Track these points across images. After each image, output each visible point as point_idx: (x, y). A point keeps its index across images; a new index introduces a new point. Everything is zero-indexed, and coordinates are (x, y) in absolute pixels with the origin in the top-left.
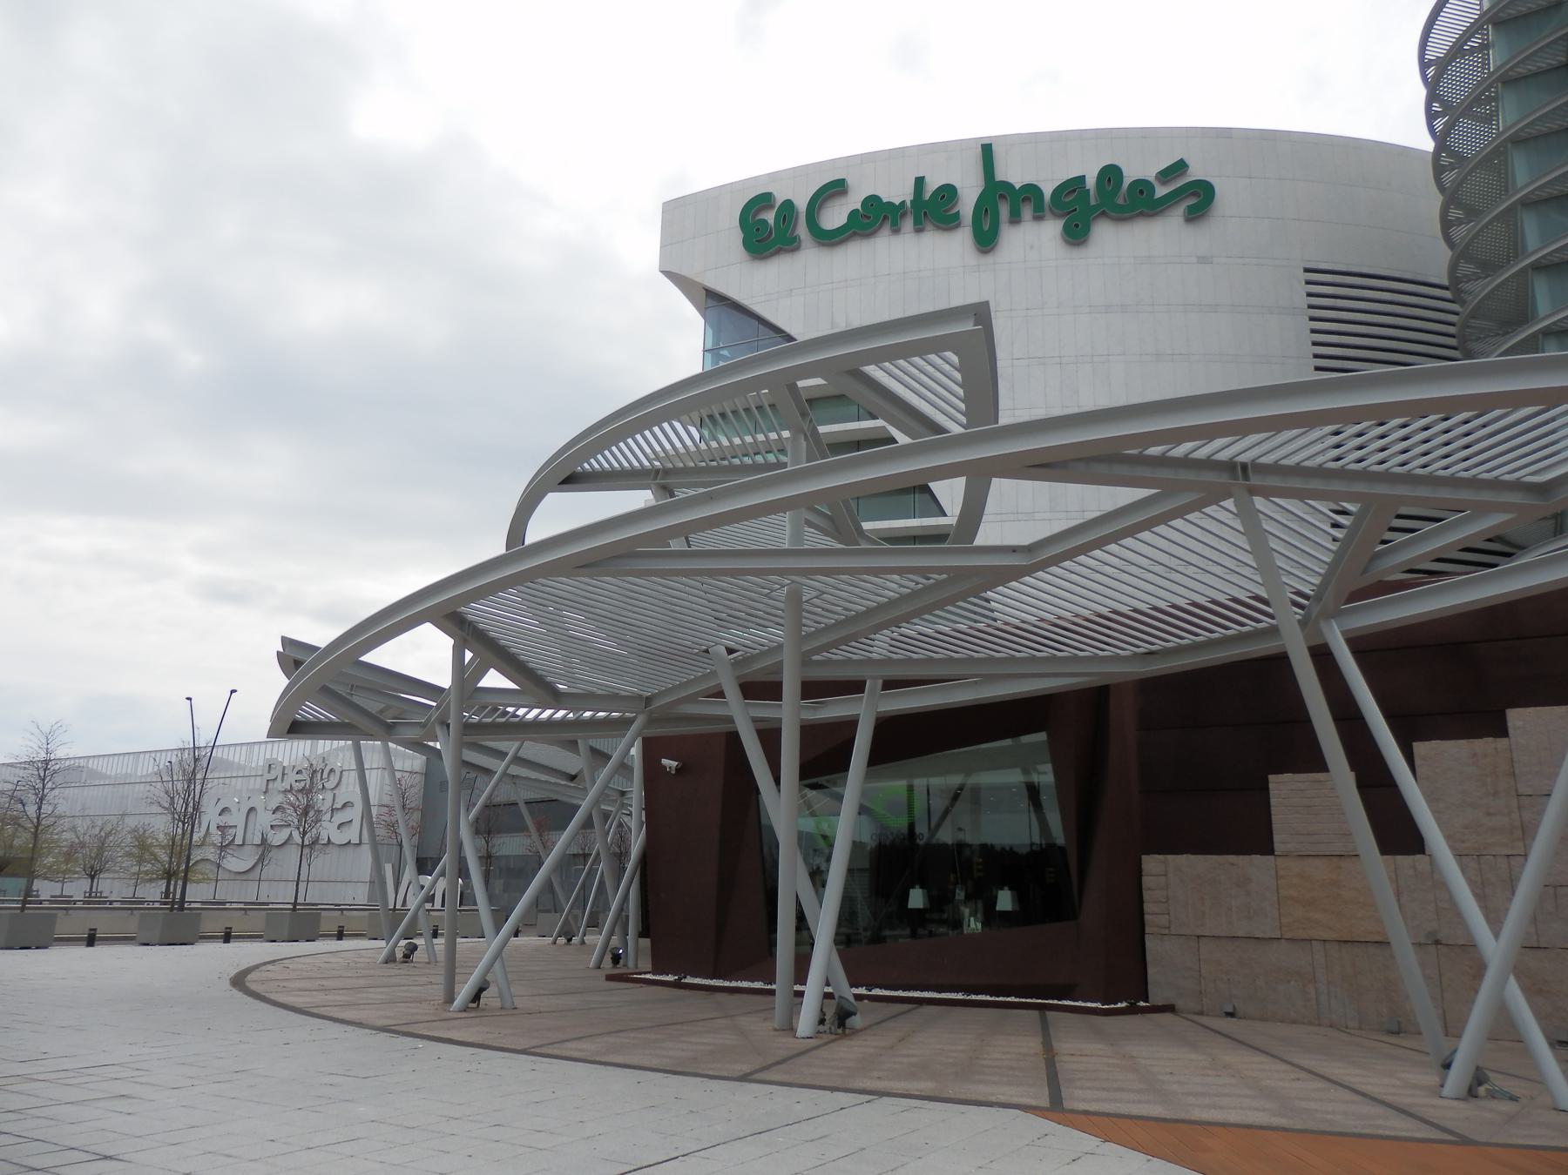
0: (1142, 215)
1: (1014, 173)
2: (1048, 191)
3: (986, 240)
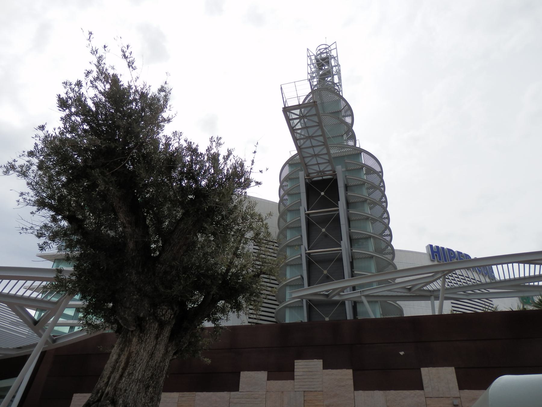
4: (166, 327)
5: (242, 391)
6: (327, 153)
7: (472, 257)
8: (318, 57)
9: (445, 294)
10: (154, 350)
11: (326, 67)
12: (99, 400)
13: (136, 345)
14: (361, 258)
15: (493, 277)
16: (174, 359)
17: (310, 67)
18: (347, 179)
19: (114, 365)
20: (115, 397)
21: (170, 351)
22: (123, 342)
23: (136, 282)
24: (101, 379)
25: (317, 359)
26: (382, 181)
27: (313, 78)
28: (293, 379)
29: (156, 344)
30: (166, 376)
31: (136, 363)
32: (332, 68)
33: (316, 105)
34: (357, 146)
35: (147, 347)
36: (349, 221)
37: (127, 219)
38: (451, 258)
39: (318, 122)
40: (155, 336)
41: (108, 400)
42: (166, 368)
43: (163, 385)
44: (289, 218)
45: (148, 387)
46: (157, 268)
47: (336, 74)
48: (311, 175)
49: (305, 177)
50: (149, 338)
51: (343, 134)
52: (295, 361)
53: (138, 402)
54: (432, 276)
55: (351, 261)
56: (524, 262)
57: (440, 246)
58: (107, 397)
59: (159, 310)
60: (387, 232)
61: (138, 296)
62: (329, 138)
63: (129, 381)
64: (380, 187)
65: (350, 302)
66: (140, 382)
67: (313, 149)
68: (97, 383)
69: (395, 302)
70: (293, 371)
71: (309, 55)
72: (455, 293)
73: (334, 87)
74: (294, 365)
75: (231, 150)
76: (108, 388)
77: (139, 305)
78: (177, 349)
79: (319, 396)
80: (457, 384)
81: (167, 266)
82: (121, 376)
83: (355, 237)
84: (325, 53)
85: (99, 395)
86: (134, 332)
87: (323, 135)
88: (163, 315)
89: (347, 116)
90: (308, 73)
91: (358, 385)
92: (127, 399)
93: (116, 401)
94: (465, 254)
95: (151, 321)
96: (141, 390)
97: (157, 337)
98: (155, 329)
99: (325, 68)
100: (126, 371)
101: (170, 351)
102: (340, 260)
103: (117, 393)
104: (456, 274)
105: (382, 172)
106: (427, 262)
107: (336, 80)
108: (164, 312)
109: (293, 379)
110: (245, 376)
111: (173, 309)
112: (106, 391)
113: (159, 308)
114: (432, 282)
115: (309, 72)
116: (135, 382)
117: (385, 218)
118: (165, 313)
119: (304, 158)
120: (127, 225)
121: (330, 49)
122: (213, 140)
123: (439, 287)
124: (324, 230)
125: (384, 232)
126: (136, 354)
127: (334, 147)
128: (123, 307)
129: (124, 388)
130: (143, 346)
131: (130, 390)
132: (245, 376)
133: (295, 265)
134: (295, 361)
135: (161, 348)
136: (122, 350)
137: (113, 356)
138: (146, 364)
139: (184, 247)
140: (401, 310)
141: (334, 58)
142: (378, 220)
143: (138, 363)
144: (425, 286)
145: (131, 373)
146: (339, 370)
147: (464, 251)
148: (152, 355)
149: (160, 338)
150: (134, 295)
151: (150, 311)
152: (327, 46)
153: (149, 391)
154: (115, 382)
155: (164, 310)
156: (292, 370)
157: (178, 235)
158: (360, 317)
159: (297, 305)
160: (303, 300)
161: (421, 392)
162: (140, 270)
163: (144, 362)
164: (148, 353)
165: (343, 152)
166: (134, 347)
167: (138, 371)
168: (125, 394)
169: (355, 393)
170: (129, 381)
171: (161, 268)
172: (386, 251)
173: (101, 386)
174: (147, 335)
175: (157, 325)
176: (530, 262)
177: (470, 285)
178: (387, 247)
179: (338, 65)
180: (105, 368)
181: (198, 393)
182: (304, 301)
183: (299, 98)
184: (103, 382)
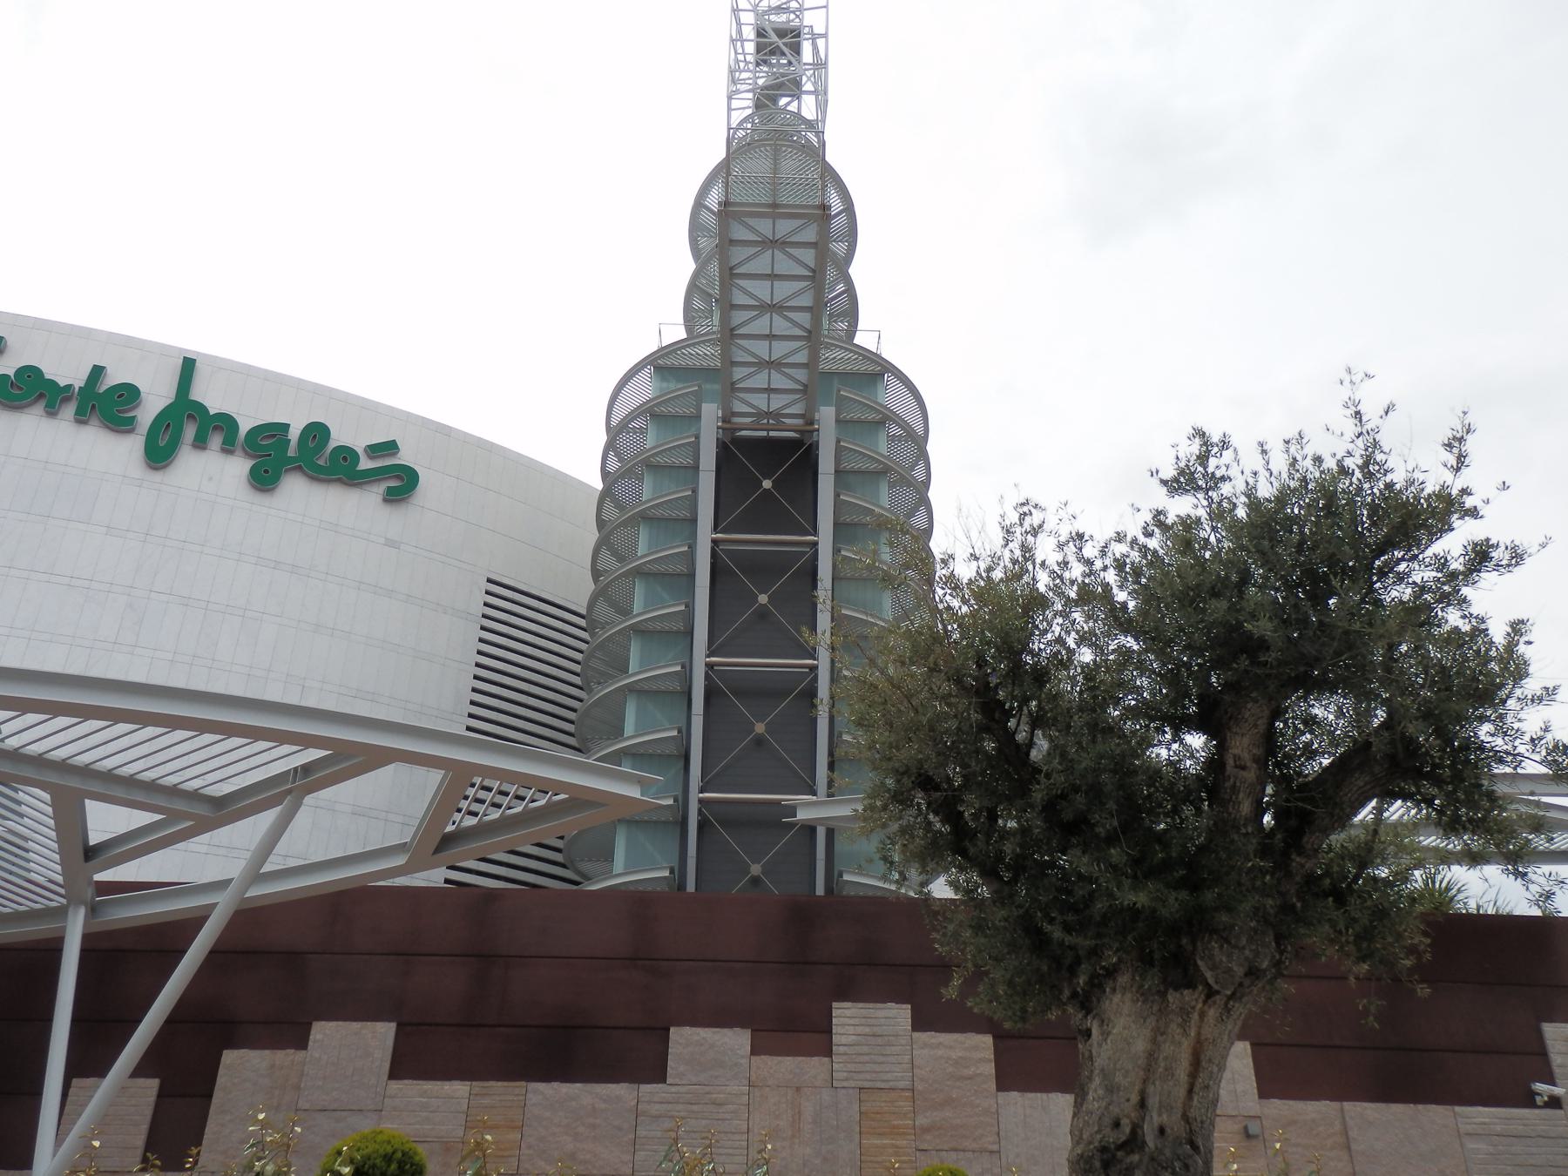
0: (339, 480)
1: (211, 396)
2: (245, 426)
3: (159, 454)
5: (677, 1081)
6: (807, 364)
25: (897, 1003)
28: (827, 1051)
39: (812, 266)
44: (644, 547)
52: (835, 1005)
79: (902, 1104)
91: (1008, 1079)
102: (811, 693)
110: (683, 1040)
128: (1225, 946)
132: (683, 1040)
133: (657, 693)
134: (835, 1005)
159: (663, 819)
169: (999, 1098)
179: (820, 65)
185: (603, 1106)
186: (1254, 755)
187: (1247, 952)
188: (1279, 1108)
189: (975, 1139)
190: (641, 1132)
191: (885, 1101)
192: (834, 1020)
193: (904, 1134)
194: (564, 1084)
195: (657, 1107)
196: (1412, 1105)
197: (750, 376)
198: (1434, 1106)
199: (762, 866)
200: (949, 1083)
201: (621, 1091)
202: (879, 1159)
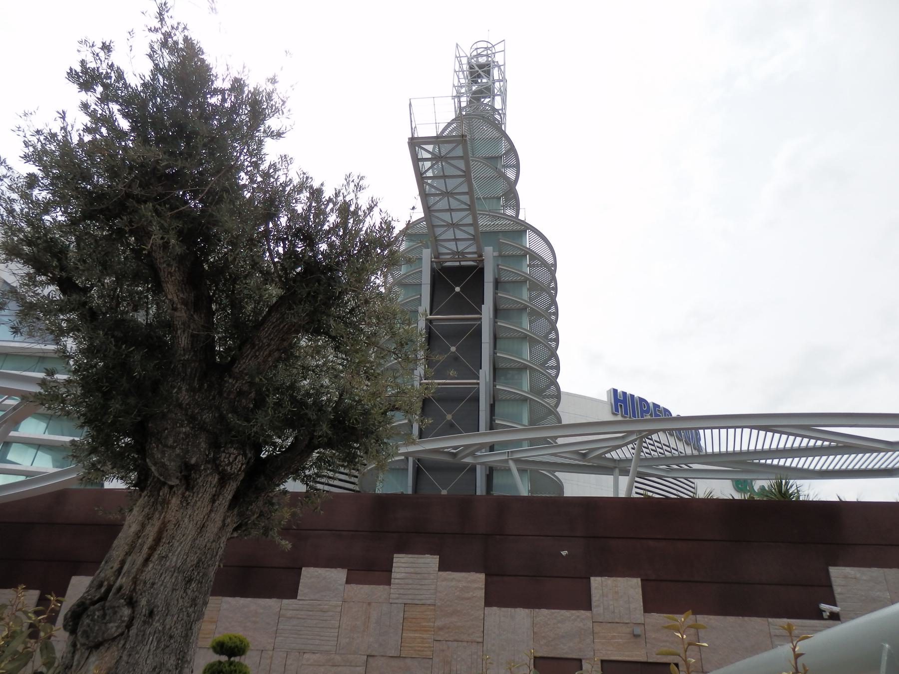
4: (230, 484)
5: (303, 598)
7: (674, 414)
8: (473, 60)
9: (639, 466)
10: (207, 520)
11: (484, 81)
12: (104, 598)
13: (177, 511)
14: (508, 400)
15: (698, 447)
16: (233, 538)
17: (458, 76)
18: (499, 270)
19: (132, 542)
20: (134, 594)
21: (228, 525)
22: (151, 504)
23: (187, 404)
24: (106, 562)
26: (554, 279)
27: (459, 96)
28: (389, 583)
29: (211, 511)
30: (219, 566)
31: (173, 541)
32: (494, 83)
33: (466, 141)
34: (521, 217)
35: (195, 514)
36: (495, 338)
37: (181, 295)
38: (643, 412)
40: (210, 496)
41: (123, 598)
42: (221, 552)
43: (213, 580)
45: (189, 581)
46: (227, 385)
47: (498, 93)
48: (441, 257)
49: (431, 258)
50: (202, 499)
51: (501, 196)
52: (395, 555)
53: (172, 604)
54: (623, 437)
55: (492, 403)
56: (759, 428)
57: (629, 392)
58: (120, 594)
59: (223, 455)
60: (552, 363)
61: (188, 429)
62: (480, 199)
63: (161, 569)
64: (549, 289)
65: (484, 467)
66: (179, 572)
67: (451, 214)
68: (97, 570)
69: (553, 472)
70: (390, 571)
71: (458, 56)
72: (650, 467)
73: (493, 115)
74: (392, 563)
75: (378, 200)
76: (122, 578)
77: (190, 443)
78: (240, 522)
79: (429, 613)
80: (642, 604)
81: (244, 382)
82: (147, 560)
83: (501, 365)
84: (485, 56)
85: (103, 590)
86: (175, 489)
87: (470, 193)
88: (230, 464)
89: (510, 166)
90: (454, 86)
91: (492, 599)
92: (155, 599)
93: (136, 602)
94: (664, 408)
95: (208, 472)
96: (180, 584)
97: (213, 500)
98: (212, 486)
99: (481, 81)
100: (156, 552)
101: (228, 525)
102: (476, 399)
103: (138, 588)
104: (651, 439)
105: (555, 265)
106: (606, 415)
107: (498, 105)
108: (231, 460)
109: (389, 583)
110: (310, 575)
111: (245, 455)
112: (117, 584)
113: (224, 452)
114: (620, 447)
115: (456, 85)
116: (171, 571)
117: (551, 340)
118: (233, 461)
119: (433, 226)
120: (179, 306)
121: (494, 51)
122: (351, 179)
123: (629, 456)
124: (453, 349)
125: (546, 362)
126: (175, 525)
127: (484, 214)
129: (151, 581)
130: (189, 513)
131: (162, 585)
135: (218, 517)
136: (149, 517)
137: (130, 527)
138: (190, 543)
139: (275, 353)
140: (560, 486)
141: (499, 67)
142: (541, 343)
143: (178, 541)
144: (609, 452)
145: (163, 557)
146: (463, 574)
147: (663, 404)
148: (202, 528)
149: (217, 502)
150: (182, 426)
151: (207, 456)
152: (490, 46)
153: (191, 587)
154: (135, 570)
155: (232, 455)
156: (388, 569)
157: (269, 332)
158: (496, 493)
160: (409, 458)
161: (588, 613)
162: (196, 385)
163: (189, 539)
164: (196, 525)
165: (497, 224)
166: (173, 514)
167: (177, 553)
168: (152, 590)
170: (161, 569)
171: (234, 386)
172: (547, 393)
173: (106, 576)
174: (198, 494)
175: (216, 480)
176: (767, 429)
177: (655, 457)
178: (548, 387)
179: (503, 80)
180: (114, 545)
181: (226, 598)
182: (411, 460)
183: (437, 125)
184: (112, 568)
185: (262, 611)
186: (182, 298)
187: (178, 451)
188: (656, 618)
189: (469, 635)
190: (281, 626)
191: (419, 612)
192: (394, 564)
193: (429, 631)
194: (243, 599)
195: (291, 612)
196: (741, 617)
197: (444, 232)
198: (756, 618)
199: (443, 489)
200: (456, 601)
201: (272, 604)
202: (411, 645)
